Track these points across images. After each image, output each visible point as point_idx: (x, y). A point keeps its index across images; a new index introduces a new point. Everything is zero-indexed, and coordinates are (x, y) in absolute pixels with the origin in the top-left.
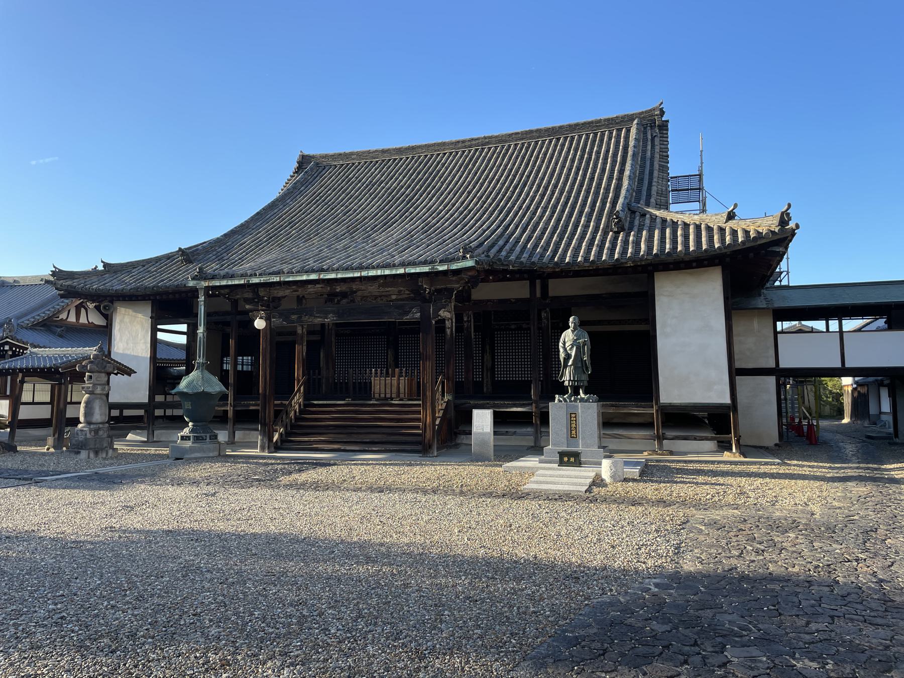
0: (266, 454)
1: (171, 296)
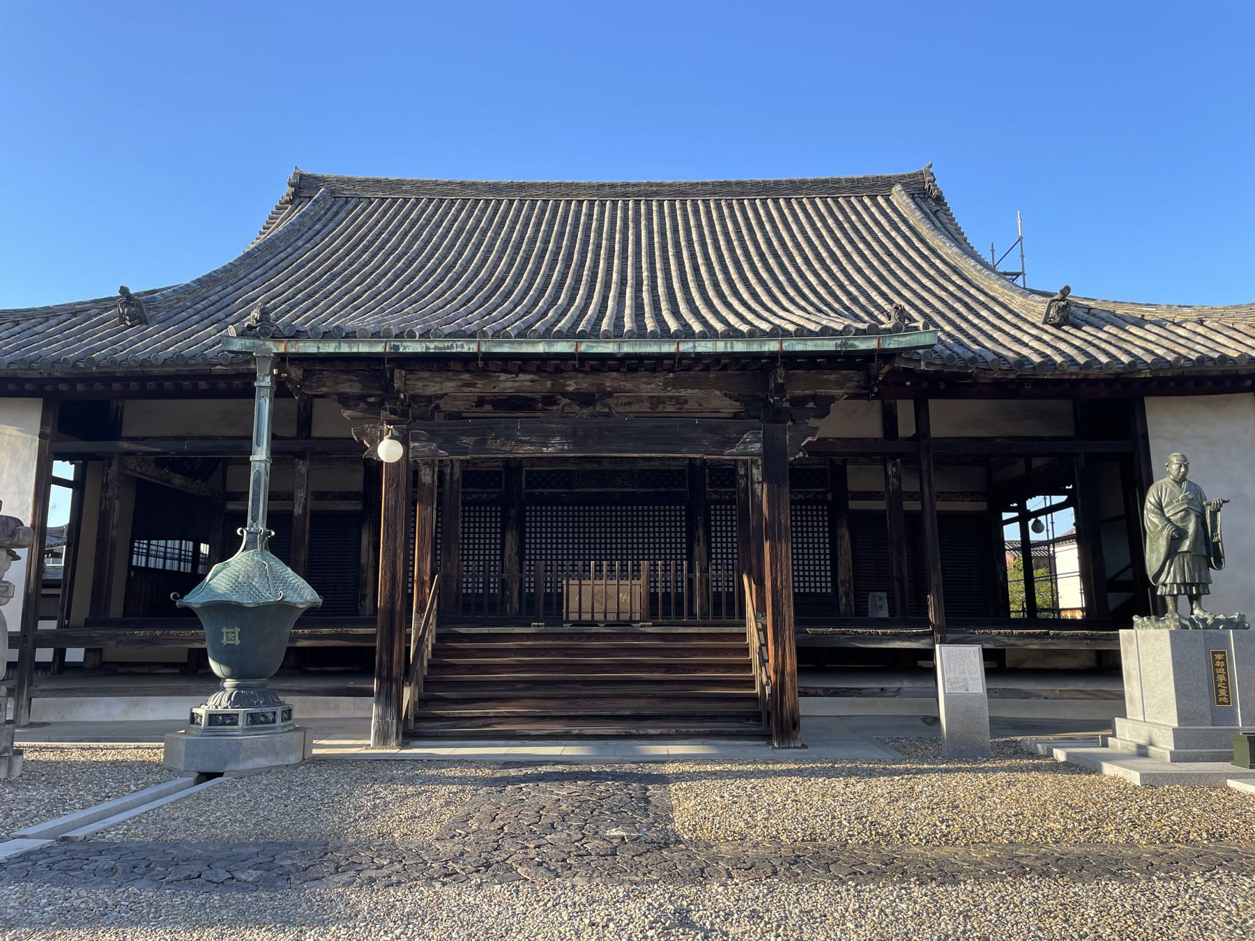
0: (393, 750)
1: (98, 386)
